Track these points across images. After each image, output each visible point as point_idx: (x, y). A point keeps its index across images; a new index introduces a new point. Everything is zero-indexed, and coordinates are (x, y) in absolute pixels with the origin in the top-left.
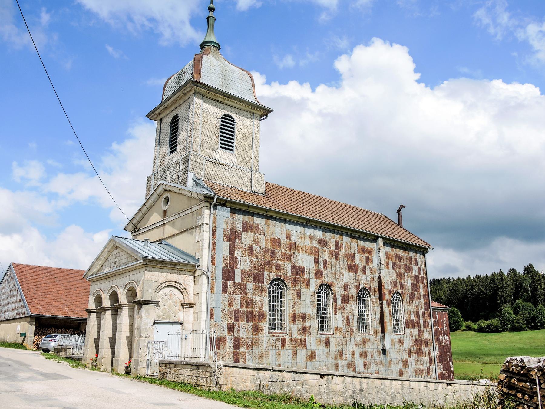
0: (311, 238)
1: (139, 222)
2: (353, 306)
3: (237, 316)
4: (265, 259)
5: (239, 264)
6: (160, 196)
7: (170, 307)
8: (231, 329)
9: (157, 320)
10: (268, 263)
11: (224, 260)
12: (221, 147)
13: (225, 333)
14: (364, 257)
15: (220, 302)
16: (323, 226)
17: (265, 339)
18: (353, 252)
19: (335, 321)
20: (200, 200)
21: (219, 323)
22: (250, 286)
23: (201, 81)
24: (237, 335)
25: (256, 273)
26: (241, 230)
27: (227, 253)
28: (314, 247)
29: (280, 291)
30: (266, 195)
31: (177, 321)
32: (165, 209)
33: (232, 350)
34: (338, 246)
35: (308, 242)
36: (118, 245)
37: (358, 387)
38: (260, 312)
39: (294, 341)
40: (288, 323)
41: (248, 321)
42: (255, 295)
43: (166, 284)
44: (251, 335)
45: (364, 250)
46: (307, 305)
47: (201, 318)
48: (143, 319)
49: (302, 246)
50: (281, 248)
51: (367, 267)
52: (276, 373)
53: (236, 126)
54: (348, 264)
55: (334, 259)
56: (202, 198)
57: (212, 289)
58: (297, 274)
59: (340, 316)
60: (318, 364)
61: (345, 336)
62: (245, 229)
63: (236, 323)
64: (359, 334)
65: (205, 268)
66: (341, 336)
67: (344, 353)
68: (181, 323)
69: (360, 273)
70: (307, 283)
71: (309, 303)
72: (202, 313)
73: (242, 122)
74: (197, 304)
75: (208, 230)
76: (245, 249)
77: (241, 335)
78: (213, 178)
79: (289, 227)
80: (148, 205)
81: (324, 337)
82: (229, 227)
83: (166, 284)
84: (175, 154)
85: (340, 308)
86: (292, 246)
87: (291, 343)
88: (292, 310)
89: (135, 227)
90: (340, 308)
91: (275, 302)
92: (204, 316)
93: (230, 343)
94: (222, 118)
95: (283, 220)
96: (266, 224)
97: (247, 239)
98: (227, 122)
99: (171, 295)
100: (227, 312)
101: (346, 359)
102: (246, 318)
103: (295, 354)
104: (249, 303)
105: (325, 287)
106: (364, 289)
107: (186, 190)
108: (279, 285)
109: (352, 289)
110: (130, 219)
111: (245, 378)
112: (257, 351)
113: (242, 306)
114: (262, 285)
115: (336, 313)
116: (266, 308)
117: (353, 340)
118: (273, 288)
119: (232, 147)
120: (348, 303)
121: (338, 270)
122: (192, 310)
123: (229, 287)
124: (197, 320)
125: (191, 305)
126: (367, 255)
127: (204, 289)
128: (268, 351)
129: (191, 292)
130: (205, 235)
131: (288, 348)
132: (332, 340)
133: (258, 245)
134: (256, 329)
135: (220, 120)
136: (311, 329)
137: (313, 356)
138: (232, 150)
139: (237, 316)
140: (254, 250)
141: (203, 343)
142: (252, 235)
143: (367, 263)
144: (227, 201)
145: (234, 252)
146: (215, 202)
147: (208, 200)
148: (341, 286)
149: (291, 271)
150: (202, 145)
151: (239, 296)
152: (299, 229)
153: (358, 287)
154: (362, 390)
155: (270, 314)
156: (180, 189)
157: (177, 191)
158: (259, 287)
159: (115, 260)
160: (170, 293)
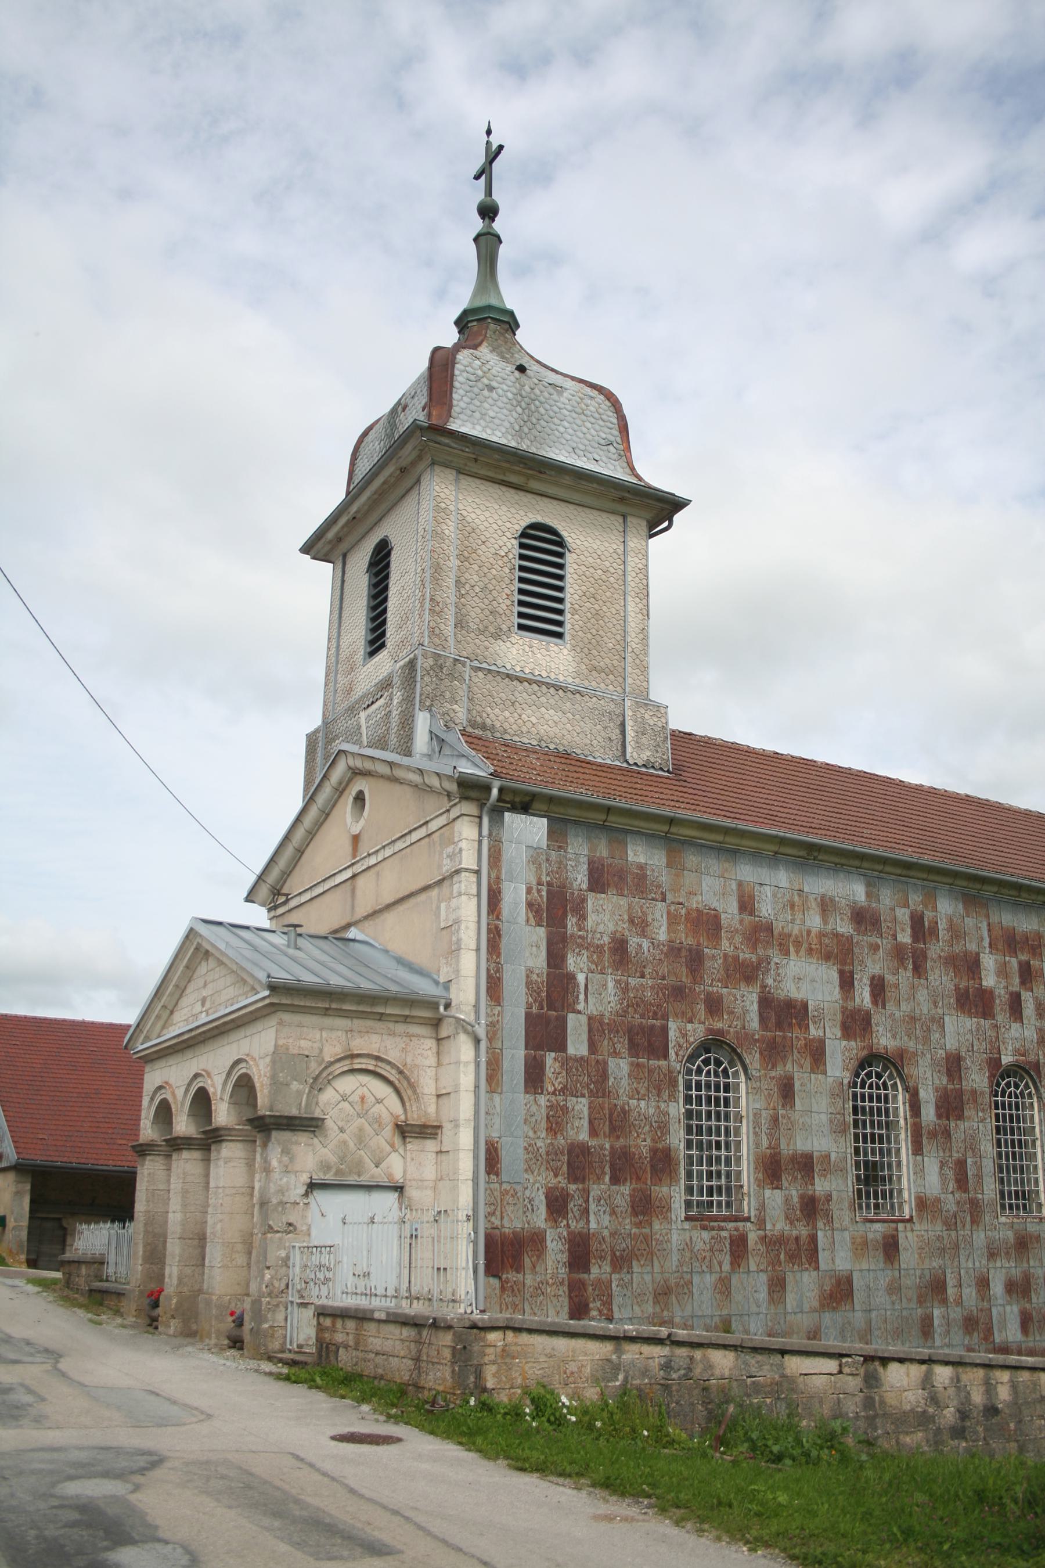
0: (826, 906)
1: (286, 875)
2: (979, 1126)
3: (578, 1163)
4: (671, 980)
5: (582, 997)
6: (340, 791)
7: (360, 1139)
8: (557, 1205)
9: (319, 1177)
10: (678, 992)
11: (529, 984)
12: (521, 627)
13: (540, 1218)
14: (1014, 961)
15: (520, 1119)
16: (865, 864)
17: (675, 1237)
18: (972, 947)
19: (917, 1176)
20: (449, 795)
21: (519, 1188)
22: (620, 1068)
23: (454, 426)
24: (576, 1225)
25: (641, 1027)
26: (585, 886)
27: (539, 961)
28: (837, 935)
29: (722, 1080)
30: (677, 770)
31: (384, 1181)
32: (355, 830)
33: (563, 1271)
34: (921, 929)
35: (815, 921)
36: (209, 948)
37: (978, 1398)
38: (654, 1151)
39: (773, 1243)
40: (753, 1187)
41: (615, 1180)
42: (636, 1094)
43: (345, 1066)
44: (628, 1225)
45: (1009, 942)
46: (818, 1126)
47: (456, 1172)
48: (276, 1176)
49: (796, 932)
50: (725, 944)
51: (1027, 997)
52: (683, 1352)
53: (570, 559)
54: (957, 988)
55: (909, 974)
56: (453, 787)
57: (492, 1074)
58: (779, 1026)
59: (931, 1164)
60: (858, 1318)
61: (951, 1224)
62: (598, 882)
63: (572, 1187)
64: (1003, 1220)
65: (466, 1014)
66: (939, 1226)
67: (951, 1281)
68: (399, 1189)
69: (1002, 1018)
70: (817, 1054)
71: (824, 1118)
72: (462, 1155)
73: (589, 544)
74: (447, 1127)
75: (474, 891)
76: (599, 949)
77: (593, 1225)
78: (498, 724)
79: (747, 872)
80: (308, 821)
81: (878, 1229)
82: (545, 879)
83: (345, 1066)
84: (383, 655)
85: (933, 1135)
86: (760, 933)
87: (762, 1248)
88: (765, 1143)
89: (276, 892)
90: (933, 1135)
91: (709, 1118)
92: (465, 1164)
93: (555, 1250)
94: (524, 535)
95: (727, 850)
96: (669, 865)
97: (604, 916)
98: (542, 547)
99: (363, 1098)
100: (543, 1151)
101: (959, 1301)
102: (607, 1169)
103: (778, 1286)
104: (614, 1121)
105: (876, 1066)
106: (1017, 1071)
107: (408, 768)
108: (719, 1063)
109: (975, 1068)
110: (258, 870)
111: (572, 1367)
112: (648, 1278)
113: (593, 1132)
114: (663, 1063)
115: (918, 1149)
116: (677, 1139)
117: (980, 1238)
118: (699, 1071)
119: (560, 624)
120: (960, 1117)
121: (925, 1008)
122: (431, 1145)
123: (549, 1072)
124: (446, 1178)
125: (427, 1131)
126: (1023, 957)
127: (467, 1079)
128: (687, 1277)
129: (426, 1091)
130: (466, 909)
131: (753, 1267)
132: (909, 1239)
133: (643, 934)
134: (645, 1207)
135: (516, 543)
136: (833, 1205)
137: (840, 1292)
138: (559, 636)
139: (578, 1163)
140: (632, 949)
141: (463, 1255)
142: (623, 902)
143: (1023, 983)
144: (534, 796)
145: (563, 958)
146: (495, 798)
147: (473, 794)
148: (934, 1063)
149: (760, 1014)
150: (460, 624)
151: (584, 1101)
152: (783, 877)
153: (994, 1063)
154: (991, 1410)
155: (690, 1157)
156: (391, 764)
157: (385, 770)
158: (650, 1071)
159: (205, 993)
160: (360, 1092)
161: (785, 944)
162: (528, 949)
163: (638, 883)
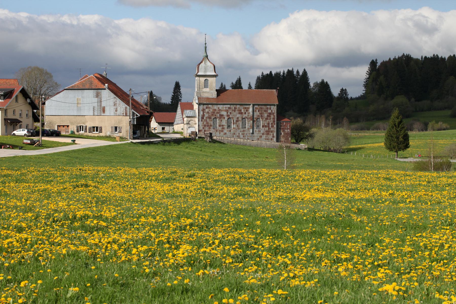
0: (226, 107)
3: (205, 126)
22: (208, 120)
39: (220, 131)
46: (224, 122)
59: (235, 125)
70: (224, 118)
79: (219, 106)
86: (220, 110)
93: (203, 131)
103: (220, 133)
104: (208, 123)
132: (232, 130)
161: (222, 111)
162: (201, 113)
163: (210, 108)
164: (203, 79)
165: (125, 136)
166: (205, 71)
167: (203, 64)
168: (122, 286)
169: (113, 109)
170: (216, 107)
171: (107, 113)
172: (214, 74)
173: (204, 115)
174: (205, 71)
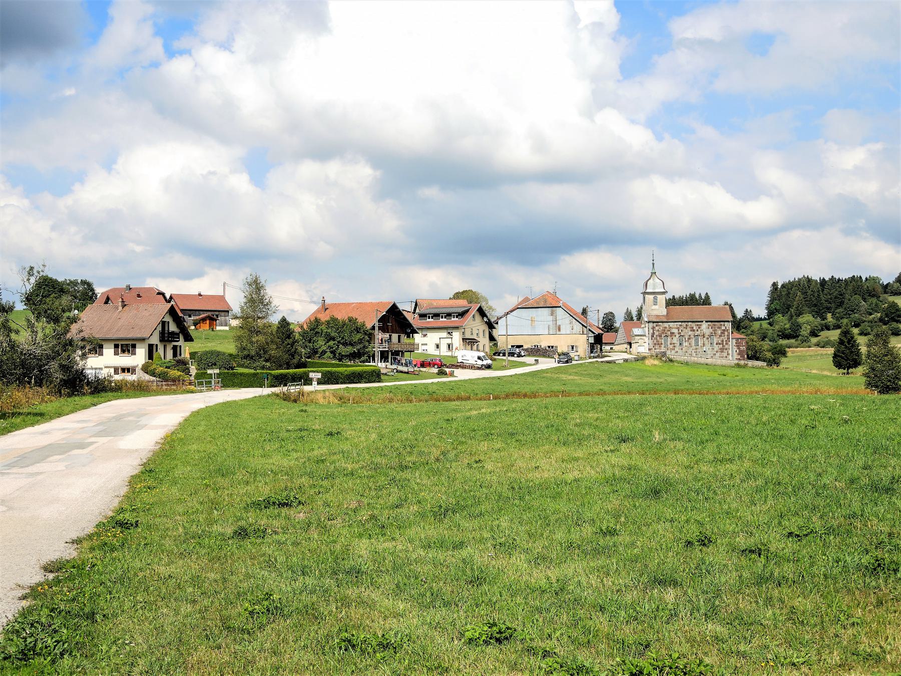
162: (651, 331)
164: (651, 297)
165: (582, 355)
166: (654, 288)
167: (651, 281)
168: (558, 493)
169: (569, 327)
170: (666, 325)
171: (562, 331)
172: (663, 290)
173: (654, 333)
174: (654, 288)
